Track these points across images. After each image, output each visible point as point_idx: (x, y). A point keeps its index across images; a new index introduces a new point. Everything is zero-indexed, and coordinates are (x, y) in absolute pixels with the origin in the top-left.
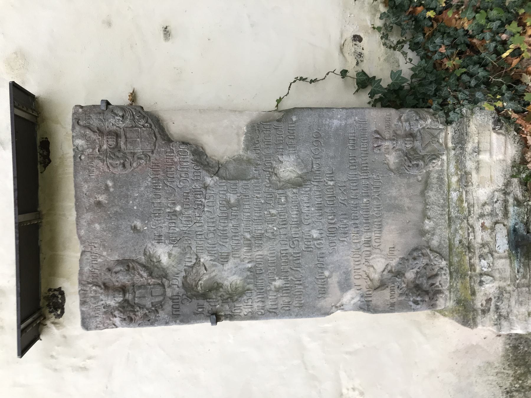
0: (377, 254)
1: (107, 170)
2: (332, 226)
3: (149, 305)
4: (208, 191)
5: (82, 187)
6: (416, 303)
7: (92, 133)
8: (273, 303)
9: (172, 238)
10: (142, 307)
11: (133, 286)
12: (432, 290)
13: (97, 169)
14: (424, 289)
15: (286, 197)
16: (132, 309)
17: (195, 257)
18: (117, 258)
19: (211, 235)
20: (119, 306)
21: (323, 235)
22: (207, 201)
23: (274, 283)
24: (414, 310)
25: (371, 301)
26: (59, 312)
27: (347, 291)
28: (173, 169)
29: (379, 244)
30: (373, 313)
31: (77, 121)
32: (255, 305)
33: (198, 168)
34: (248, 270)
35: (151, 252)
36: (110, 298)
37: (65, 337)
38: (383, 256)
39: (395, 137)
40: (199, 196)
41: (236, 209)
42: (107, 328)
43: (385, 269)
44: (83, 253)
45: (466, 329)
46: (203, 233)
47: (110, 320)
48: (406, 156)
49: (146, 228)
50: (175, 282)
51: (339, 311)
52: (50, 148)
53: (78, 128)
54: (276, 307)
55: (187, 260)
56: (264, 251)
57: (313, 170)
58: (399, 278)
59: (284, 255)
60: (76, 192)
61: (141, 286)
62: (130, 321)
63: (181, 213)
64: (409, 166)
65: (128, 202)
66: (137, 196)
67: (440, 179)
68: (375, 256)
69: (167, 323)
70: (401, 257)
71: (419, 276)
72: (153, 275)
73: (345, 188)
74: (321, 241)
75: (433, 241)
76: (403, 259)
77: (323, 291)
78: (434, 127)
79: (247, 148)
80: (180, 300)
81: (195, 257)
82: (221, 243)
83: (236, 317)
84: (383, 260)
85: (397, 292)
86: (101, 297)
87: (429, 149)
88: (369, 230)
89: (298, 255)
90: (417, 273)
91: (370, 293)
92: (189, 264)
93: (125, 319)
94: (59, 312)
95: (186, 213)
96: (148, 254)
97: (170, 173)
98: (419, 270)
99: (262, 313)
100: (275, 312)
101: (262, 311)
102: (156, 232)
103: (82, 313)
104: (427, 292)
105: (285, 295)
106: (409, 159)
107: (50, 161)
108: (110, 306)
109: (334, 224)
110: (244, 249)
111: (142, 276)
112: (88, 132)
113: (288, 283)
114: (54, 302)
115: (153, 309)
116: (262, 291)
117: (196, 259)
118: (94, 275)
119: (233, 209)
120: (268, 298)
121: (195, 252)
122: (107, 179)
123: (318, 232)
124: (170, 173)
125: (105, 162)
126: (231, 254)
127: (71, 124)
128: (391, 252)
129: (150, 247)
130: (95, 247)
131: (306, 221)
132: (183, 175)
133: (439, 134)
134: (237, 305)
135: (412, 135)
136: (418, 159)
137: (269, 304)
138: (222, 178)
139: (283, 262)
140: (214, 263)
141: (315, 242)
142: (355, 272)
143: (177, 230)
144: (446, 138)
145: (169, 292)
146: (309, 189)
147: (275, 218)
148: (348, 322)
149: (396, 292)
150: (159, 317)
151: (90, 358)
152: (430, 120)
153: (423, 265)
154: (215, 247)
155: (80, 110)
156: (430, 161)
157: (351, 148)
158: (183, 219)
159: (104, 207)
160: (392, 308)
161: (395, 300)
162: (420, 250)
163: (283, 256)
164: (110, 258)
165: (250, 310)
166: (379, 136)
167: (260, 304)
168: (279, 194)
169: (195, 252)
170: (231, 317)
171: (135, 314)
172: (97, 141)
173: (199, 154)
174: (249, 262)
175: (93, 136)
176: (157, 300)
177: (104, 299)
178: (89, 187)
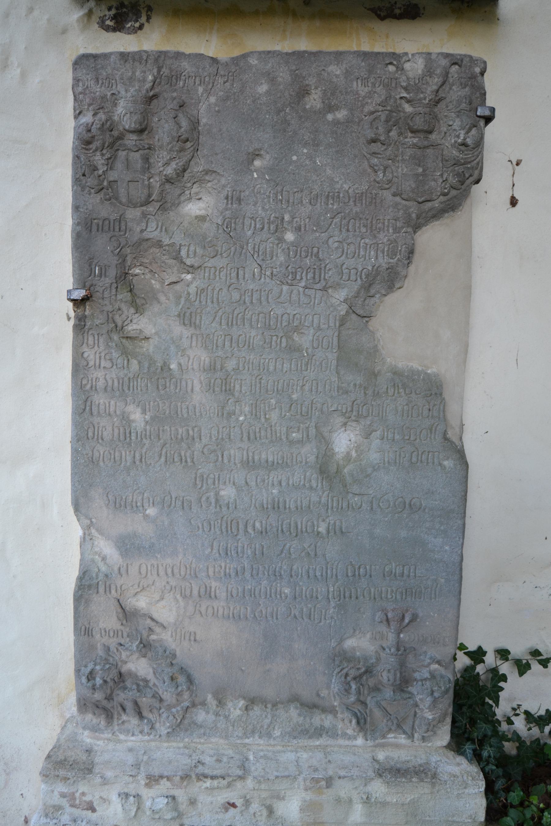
0: (185, 608)
1: (366, 109)
2: (241, 526)
3: (113, 175)
4: (319, 294)
5: (337, 65)
6: (91, 676)
7: (435, 87)
8: (102, 407)
9: (235, 223)
10: (110, 163)
11: (149, 148)
12: (113, 707)
13: (370, 92)
14: (116, 692)
15: (301, 442)
16: (106, 146)
17: (196, 265)
18: (203, 121)
19: (236, 296)
20: (113, 122)
21: (224, 509)
22: (301, 290)
23: (139, 410)
24: (78, 671)
25: (98, 592)
26: (108, 22)
27: (119, 548)
28: (363, 230)
29: (203, 612)
30: (74, 595)
31: (456, 61)
32: (100, 374)
33: (364, 277)
34: (165, 363)
35: (209, 185)
36: (130, 105)
37: (64, 31)
38: (180, 619)
39: (402, 651)
40: (310, 275)
41: (284, 345)
42: (75, 100)
43: (157, 622)
44: (214, 60)
45: (40, 764)
46: (241, 281)
47: (90, 105)
48: (366, 672)
49: (256, 176)
50: (152, 225)
51: (80, 533)
52: (406, 20)
53: (444, 62)
54: (95, 412)
55: (192, 248)
56: (199, 397)
57: (351, 495)
58: (138, 647)
59: (191, 432)
60: (330, 53)
61: (149, 164)
62: (85, 142)
63: (281, 240)
64: (347, 675)
65: (306, 145)
66: (315, 162)
67: (320, 732)
68: (182, 604)
69: (76, 208)
70: (178, 653)
71: (141, 683)
72: (167, 186)
73: (312, 554)
74: (213, 504)
75: (204, 713)
76: (174, 656)
77: (119, 505)
78: (417, 722)
79: (396, 372)
80: (116, 234)
81: (196, 265)
82: (220, 313)
83: (81, 337)
84: (172, 620)
85: (113, 643)
86: (132, 90)
87: (378, 713)
88: (230, 596)
89: (189, 460)
90: (146, 681)
91: (113, 592)
92: (183, 253)
93: (89, 131)
94: (108, 22)
95: (279, 251)
96: (207, 178)
97: (357, 225)
98: (151, 684)
99: (86, 385)
100: (84, 410)
101: (88, 387)
102: (247, 193)
103: (106, 56)
104: (109, 698)
105: (116, 431)
106: (361, 676)
107: (382, 18)
108: (115, 105)
109: (246, 531)
110: (205, 357)
111: (167, 164)
112: (437, 80)
113: (137, 438)
114: (128, 14)
115: (105, 183)
116: (126, 389)
117: (192, 266)
118: (174, 81)
119: (284, 340)
120: (112, 398)
121: (205, 265)
122: (351, 110)
123: (232, 500)
124: (357, 225)
125: (380, 108)
126: (198, 332)
127: (451, 51)
128: (187, 636)
129: (219, 181)
130: (225, 83)
131: (254, 478)
132: (352, 248)
133: (405, 732)
134: (101, 340)
135: (403, 684)
136: (359, 693)
137: (100, 399)
138: (343, 321)
139: (177, 430)
140: (183, 300)
141: (212, 494)
142: (152, 565)
143: (250, 233)
144: (397, 746)
145: (132, 214)
146: (314, 485)
147: (263, 420)
148: (59, 546)
149: (111, 640)
150: (90, 194)
151: (23, 75)
152: (430, 717)
153: (160, 693)
154: (212, 302)
155: (477, 70)
156: (355, 715)
157: (387, 569)
158: (269, 245)
159: (299, 102)
160: (83, 630)
161: (98, 637)
162: (189, 689)
163: (188, 430)
164: (203, 108)
165: (91, 363)
166: (407, 621)
167: (101, 384)
168: (308, 428)
169: (205, 265)
170: (81, 327)
171: (96, 150)
172: (422, 96)
173: (390, 279)
174: (180, 364)
175: (429, 89)
176: (122, 192)
177: (129, 95)
178: (337, 76)
